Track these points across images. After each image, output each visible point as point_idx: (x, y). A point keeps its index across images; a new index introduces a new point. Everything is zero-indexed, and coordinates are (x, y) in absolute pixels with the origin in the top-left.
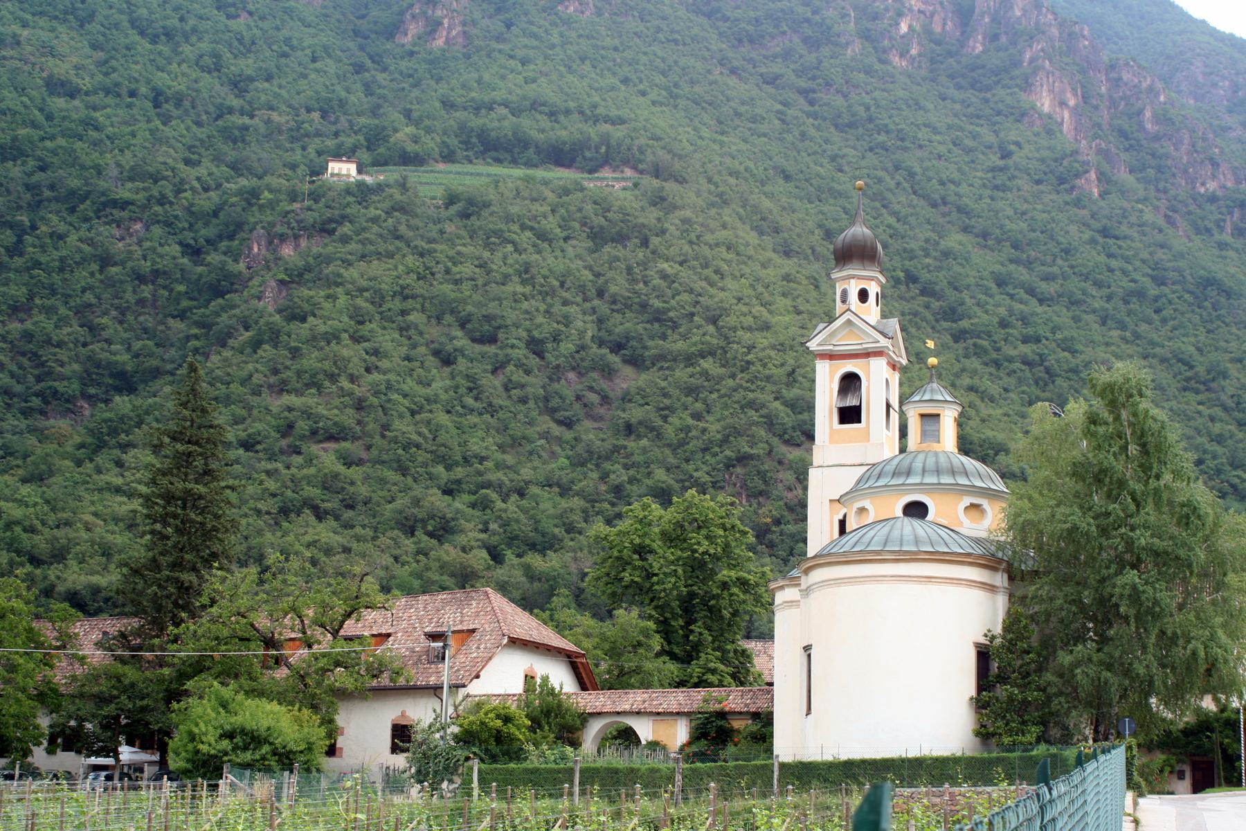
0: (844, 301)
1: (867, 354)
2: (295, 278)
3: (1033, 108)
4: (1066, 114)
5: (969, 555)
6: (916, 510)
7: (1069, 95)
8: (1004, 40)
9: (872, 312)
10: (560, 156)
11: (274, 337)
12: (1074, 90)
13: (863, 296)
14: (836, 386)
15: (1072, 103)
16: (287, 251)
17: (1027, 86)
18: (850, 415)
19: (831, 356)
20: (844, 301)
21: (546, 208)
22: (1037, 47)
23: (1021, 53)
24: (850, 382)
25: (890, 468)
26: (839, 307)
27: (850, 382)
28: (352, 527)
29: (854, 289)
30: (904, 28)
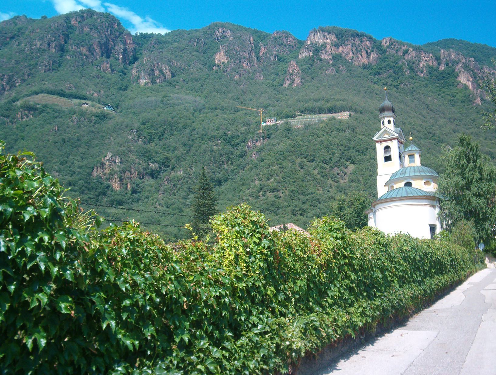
0: (383, 124)
1: (391, 140)
2: (261, 150)
3: (460, 82)
4: (470, 83)
5: (424, 196)
6: (408, 184)
7: (470, 78)
8: (450, 65)
9: (391, 127)
10: (330, 111)
11: (256, 166)
12: (471, 76)
13: (389, 122)
14: (383, 151)
15: (471, 80)
16: (258, 144)
17: (457, 76)
18: (388, 159)
19: (381, 142)
20: (383, 124)
21: (325, 125)
22: (460, 65)
23: (455, 67)
24: (387, 148)
25: (399, 173)
26: (382, 126)
27: (387, 148)
28: (279, 214)
29: (386, 120)
30: (421, 65)
